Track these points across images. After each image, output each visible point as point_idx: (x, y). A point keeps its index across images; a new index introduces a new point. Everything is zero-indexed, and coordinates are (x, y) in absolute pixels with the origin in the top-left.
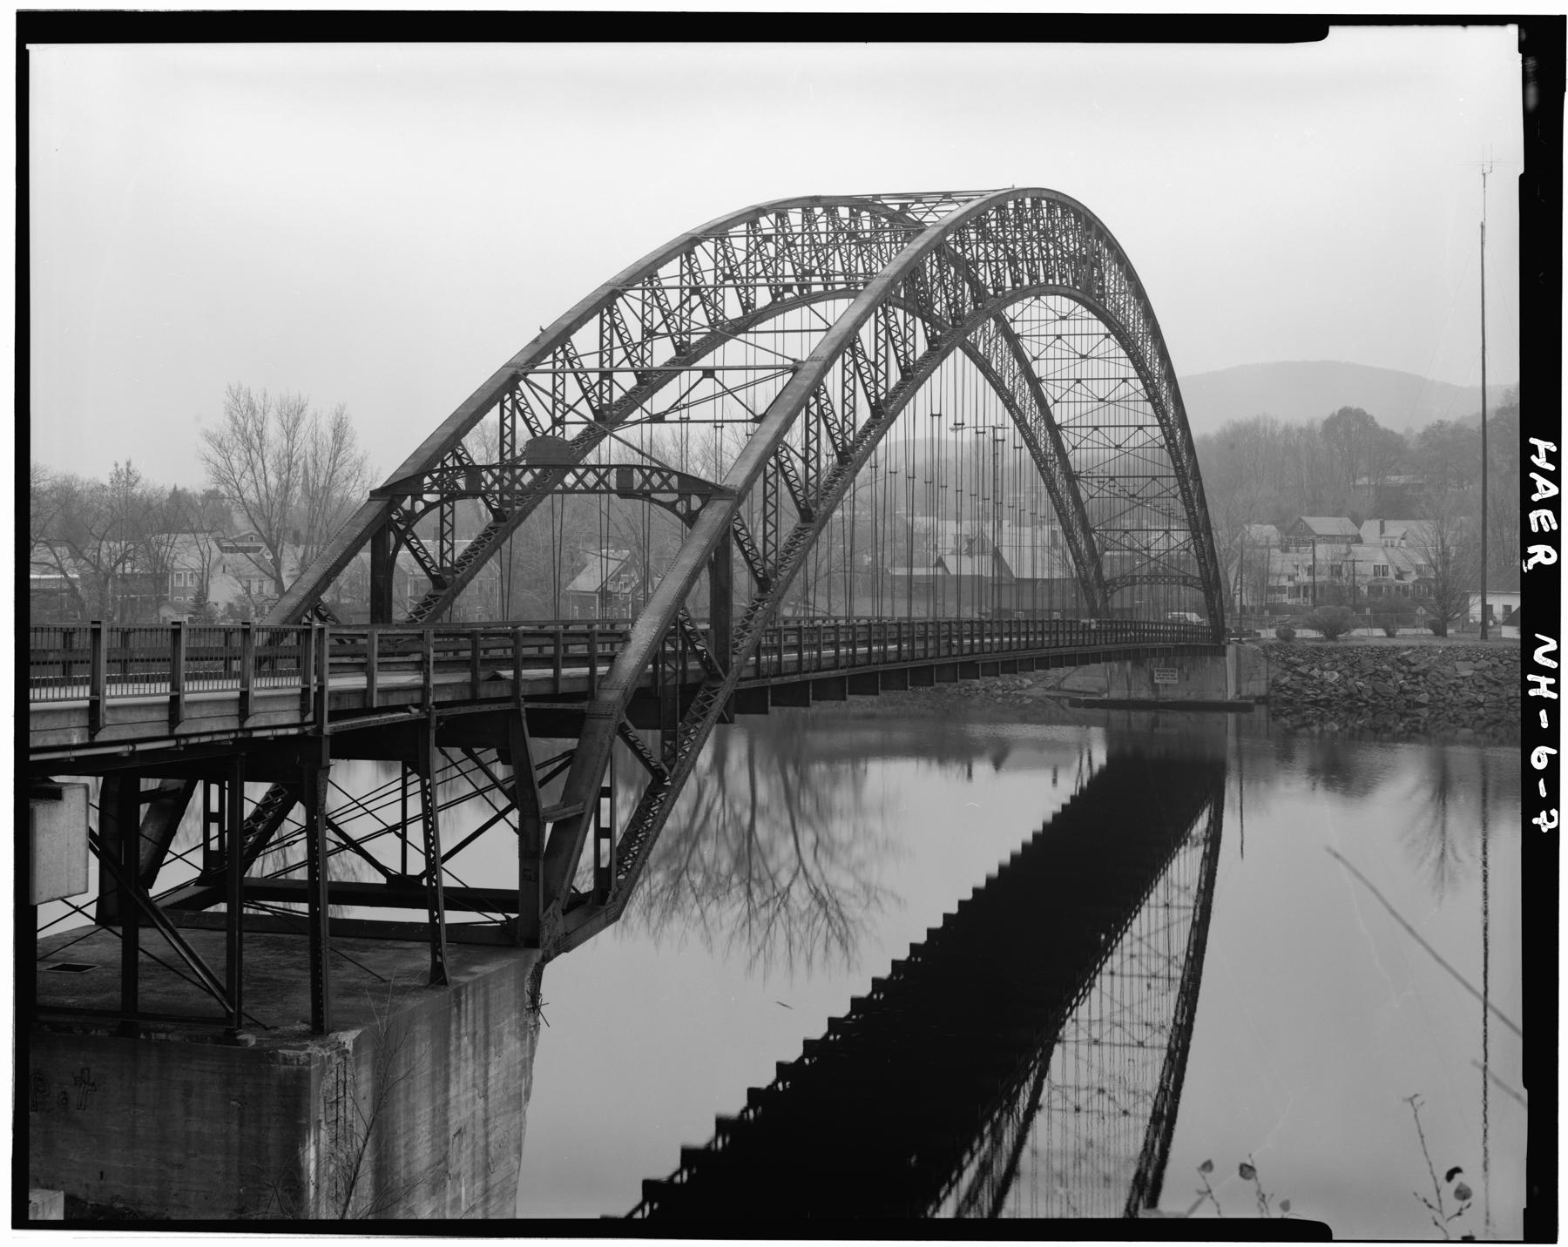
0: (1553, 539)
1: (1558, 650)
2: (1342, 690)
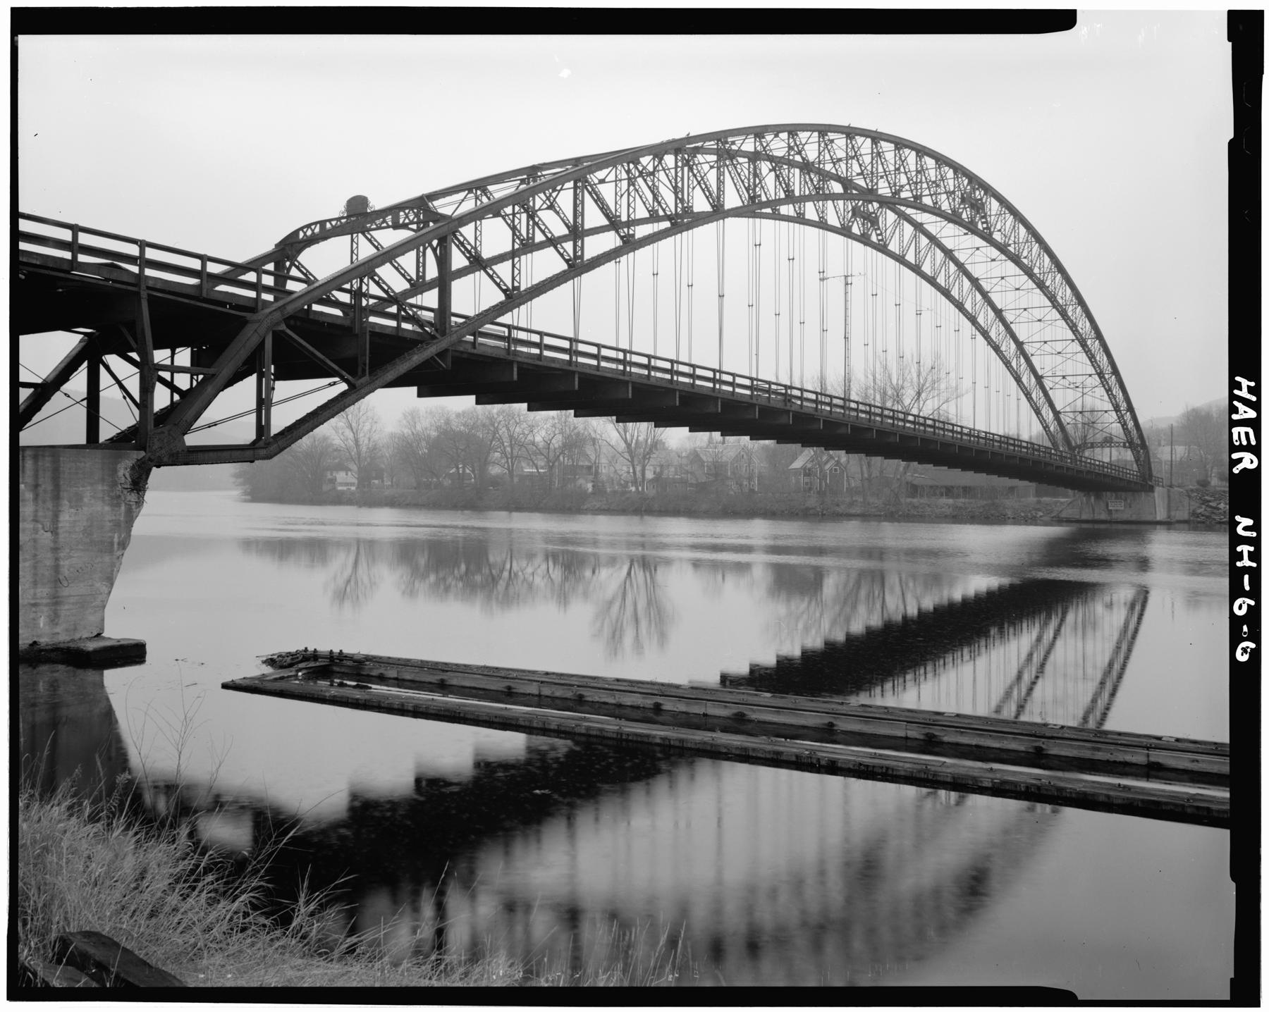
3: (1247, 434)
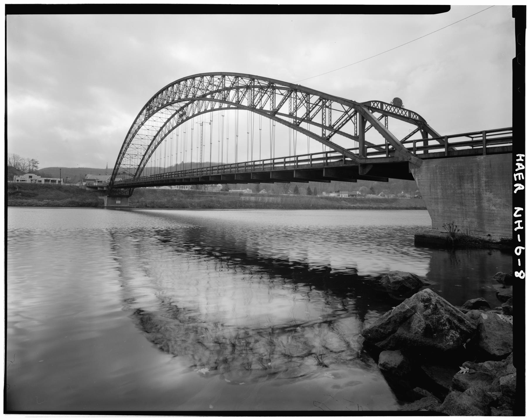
0: (523, 182)
1: (524, 169)
3: (521, 175)
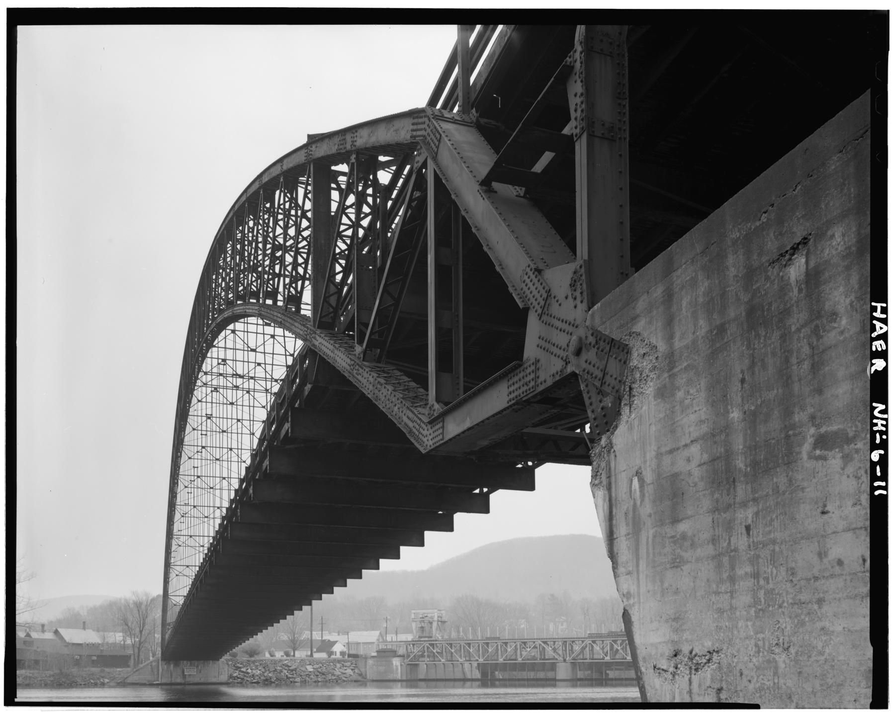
2: (263, 678)
